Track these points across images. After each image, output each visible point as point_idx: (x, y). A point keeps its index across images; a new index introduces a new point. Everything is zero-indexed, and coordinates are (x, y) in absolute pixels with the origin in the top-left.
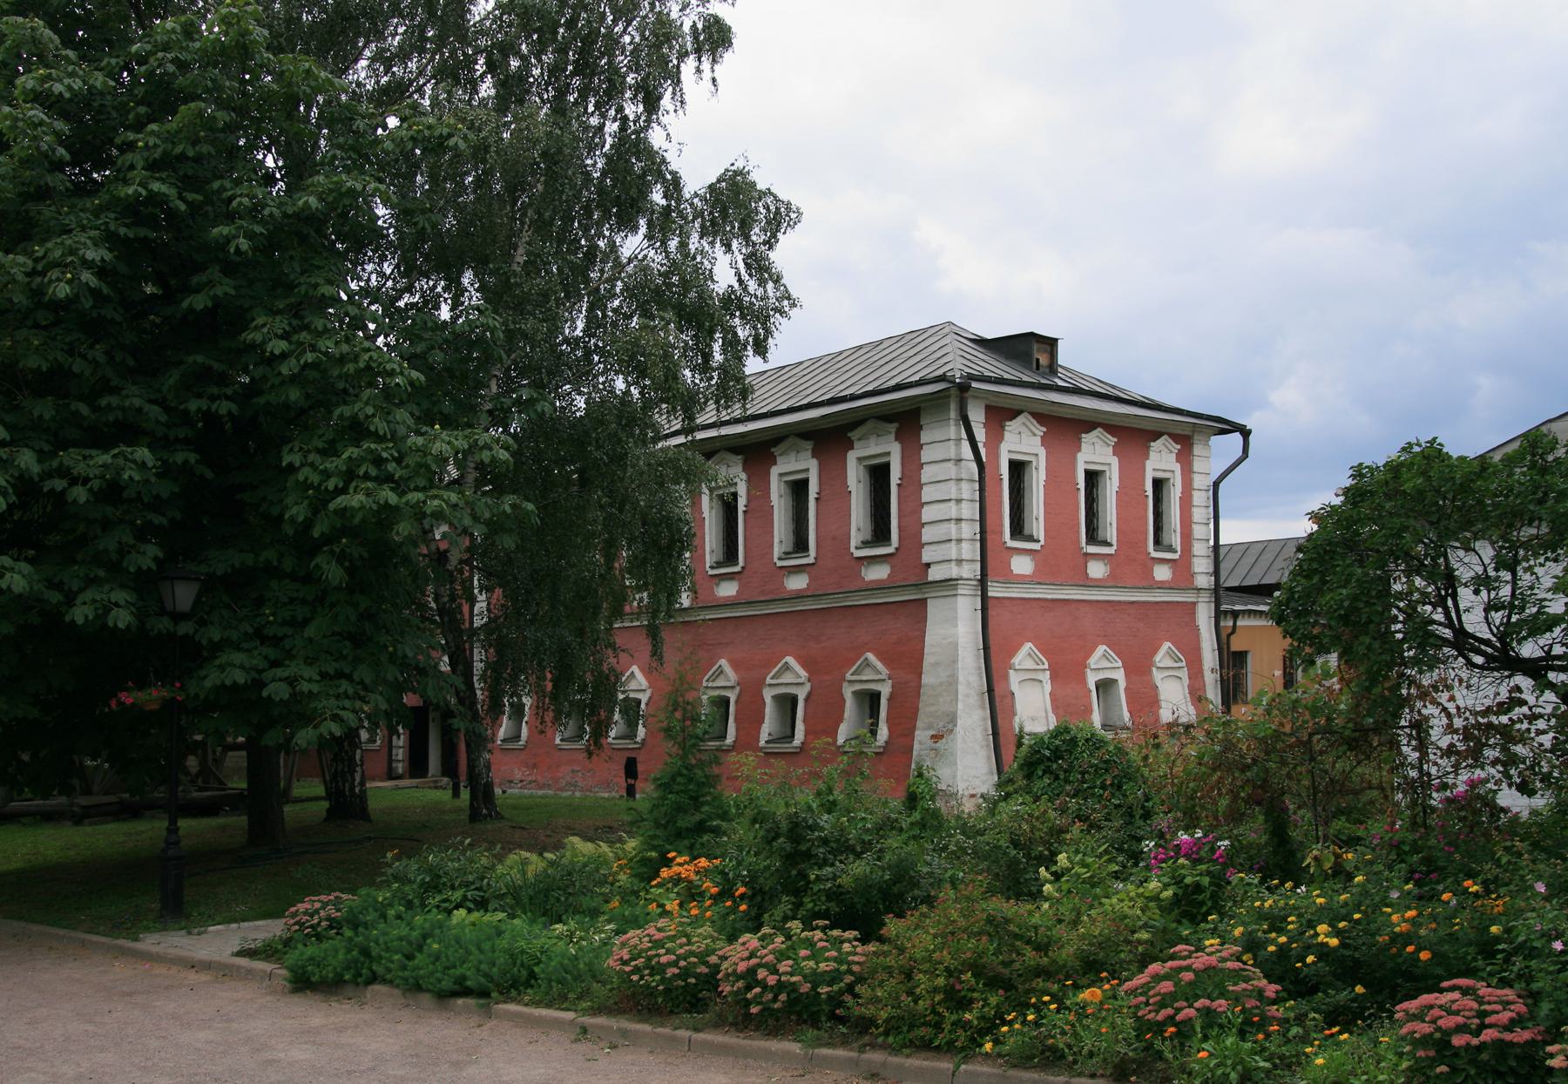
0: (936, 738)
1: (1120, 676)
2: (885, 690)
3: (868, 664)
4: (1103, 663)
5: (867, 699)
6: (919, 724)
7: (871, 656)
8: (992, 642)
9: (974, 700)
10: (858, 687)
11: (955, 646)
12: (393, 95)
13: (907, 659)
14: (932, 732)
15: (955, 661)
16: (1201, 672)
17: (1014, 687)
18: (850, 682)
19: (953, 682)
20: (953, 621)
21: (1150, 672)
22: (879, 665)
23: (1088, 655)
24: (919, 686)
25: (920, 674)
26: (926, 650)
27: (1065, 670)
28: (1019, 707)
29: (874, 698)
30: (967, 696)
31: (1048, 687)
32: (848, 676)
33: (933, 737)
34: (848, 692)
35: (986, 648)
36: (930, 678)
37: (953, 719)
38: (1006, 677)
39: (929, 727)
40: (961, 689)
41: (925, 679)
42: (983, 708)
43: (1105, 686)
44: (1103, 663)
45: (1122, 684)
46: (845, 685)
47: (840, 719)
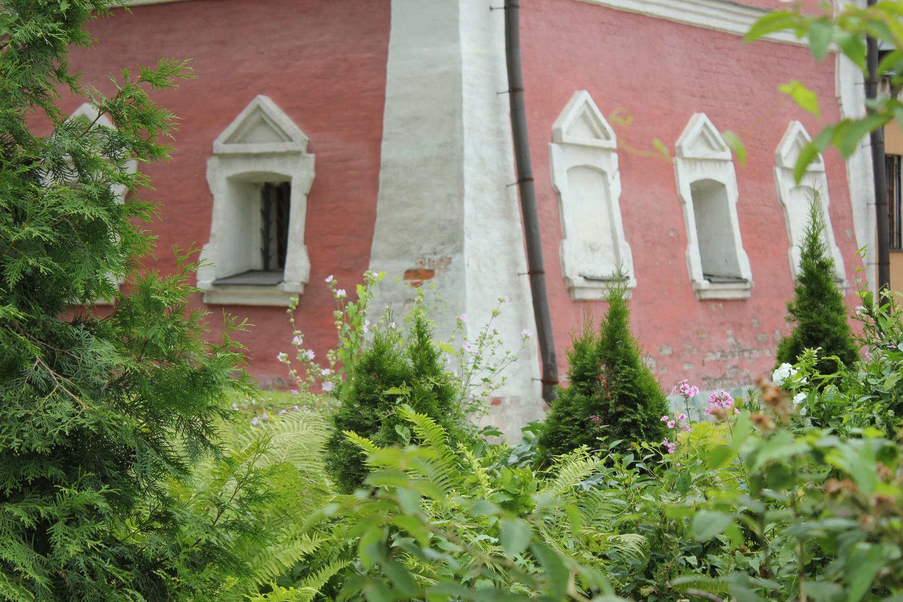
0: (418, 275)
1: (726, 176)
2: (301, 177)
3: (264, 121)
4: (702, 152)
5: (257, 197)
6: (377, 246)
7: (266, 102)
8: (526, 81)
9: (491, 198)
10: (241, 168)
11: (454, 80)
12: (114, 326)
13: (349, 112)
14: (412, 265)
15: (455, 113)
16: (845, 185)
17: (561, 180)
18: (223, 157)
19: (450, 158)
20: (449, 29)
21: (772, 174)
22: (287, 122)
23: (677, 132)
24: (376, 165)
25: (377, 141)
26: (390, 92)
27: (644, 165)
28: (569, 220)
29: (274, 197)
30: (481, 188)
31: (616, 187)
32: (219, 145)
33: (410, 274)
34: (219, 179)
35: (514, 90)
36: (400, 150)
37: (453, 236)
38: (546, 157)
39: (401, 253)
40: (470, 171)
41: (389, 152)
42: (507, 215)
43: (705, 192)
44: (702, 152)
45: (732, 194)
46: (212, 163)
47: (202, 235)
